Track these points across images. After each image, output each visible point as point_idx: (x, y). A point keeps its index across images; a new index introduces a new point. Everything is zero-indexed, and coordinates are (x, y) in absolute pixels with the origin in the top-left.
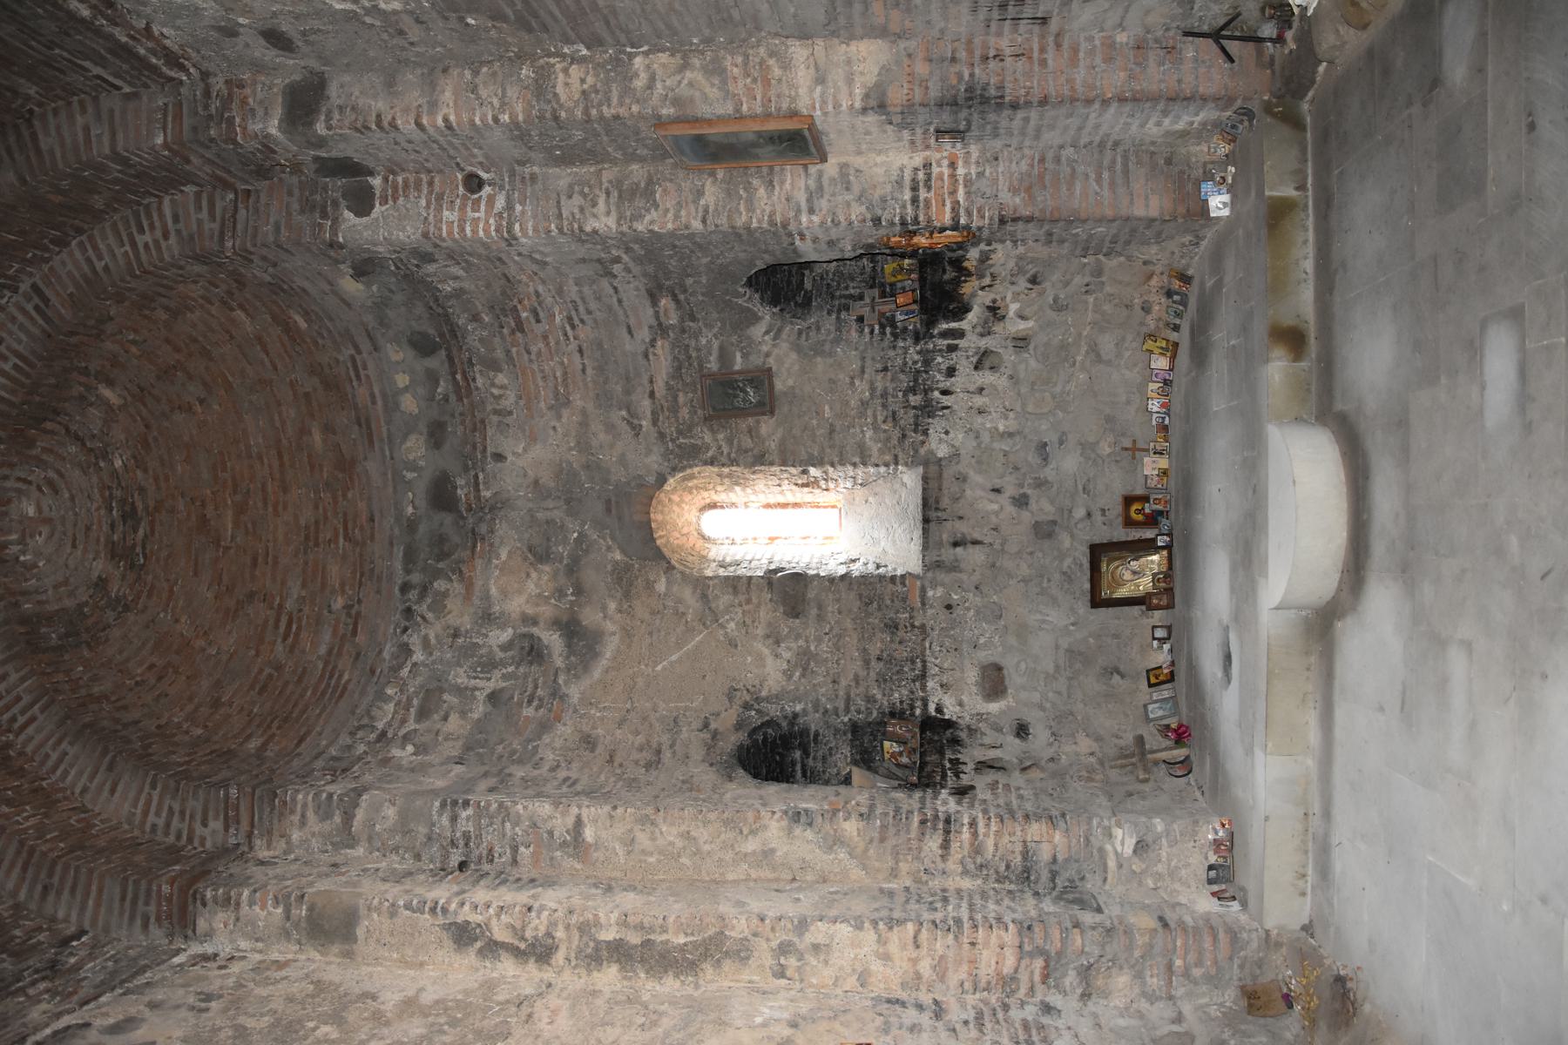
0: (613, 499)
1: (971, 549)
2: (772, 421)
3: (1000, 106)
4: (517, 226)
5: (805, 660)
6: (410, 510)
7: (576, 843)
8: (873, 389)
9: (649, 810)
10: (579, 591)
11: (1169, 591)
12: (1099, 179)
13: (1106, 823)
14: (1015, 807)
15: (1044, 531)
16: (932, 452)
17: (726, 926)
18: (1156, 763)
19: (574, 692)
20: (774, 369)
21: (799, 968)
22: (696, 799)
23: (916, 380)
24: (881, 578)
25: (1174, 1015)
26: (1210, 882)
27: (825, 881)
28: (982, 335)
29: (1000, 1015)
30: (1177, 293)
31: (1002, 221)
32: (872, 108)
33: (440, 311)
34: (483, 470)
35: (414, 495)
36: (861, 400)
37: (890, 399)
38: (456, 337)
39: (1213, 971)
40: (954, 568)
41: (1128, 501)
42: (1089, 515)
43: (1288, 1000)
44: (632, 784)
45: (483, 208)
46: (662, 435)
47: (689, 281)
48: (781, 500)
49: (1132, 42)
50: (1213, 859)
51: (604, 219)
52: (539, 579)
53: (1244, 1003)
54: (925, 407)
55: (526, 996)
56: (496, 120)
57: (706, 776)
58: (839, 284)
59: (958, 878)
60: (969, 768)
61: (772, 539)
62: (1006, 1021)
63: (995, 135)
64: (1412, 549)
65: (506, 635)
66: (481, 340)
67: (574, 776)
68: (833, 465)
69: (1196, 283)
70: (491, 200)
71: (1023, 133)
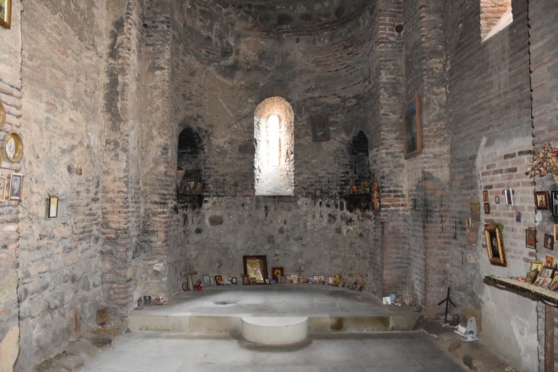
0: (282, 83)
1: (264, 213)
2: (310, 141)
3: (424, 222)
4: (383, 45)
5: (223, 153)
6: (278, 7)
7: (154, 68)
8: (322, 177)
9: (167, 95)
10: (248, 70)
11: (249, 283)
12: (397, 258)
13: (165, 260)
14: (170, 228)
15: (271, 239)
16: (299, 199)
17: (124, 122)
18: (187, 279)
19: (211, 68)
20: (330, 142)
21: (109, 149)
22: (171, 112)
23: (325, 193)
24: (254, 181)
25: (96, 284)
26: (145, 297)
27: (142, 159)
28: (341, 217)
29: (94, 222)
30: (356, 286)
31: (382, 223)
32: (424, 175)
33: (352, 18)
34: (293, 35)
35: (284, 9)
36: (318, 173)
37: (318, 184)
38: (342, 24)
39: (112, 298)
40: (257, 207)
41: (282, 269)
42: (277, 255)
43: (103, 324)
44: (177, 89)
45: (390, 32)
46: (305, 100)
47: (362, 110)
48: (282, 145)
49: (446, 269)
50: (153, 298)
51: (385, 77)
52: (253, 56)
53: (101, 309)
54: (316, 196)
55: (96, 48)
56: (423, 36)
57: (180, 116)
58: (360, 165)
59: (144, 207)
60: (185, 212)
61: (268, 142)
62: (92, 224)
63: (414, 220)
64: (262, 366)
65: (232, 43)
66: (341, 33)
67: (180, 68)
68: (294, 163)
69: (360, 293)
70: (393, 35)
71: (414, 230)
